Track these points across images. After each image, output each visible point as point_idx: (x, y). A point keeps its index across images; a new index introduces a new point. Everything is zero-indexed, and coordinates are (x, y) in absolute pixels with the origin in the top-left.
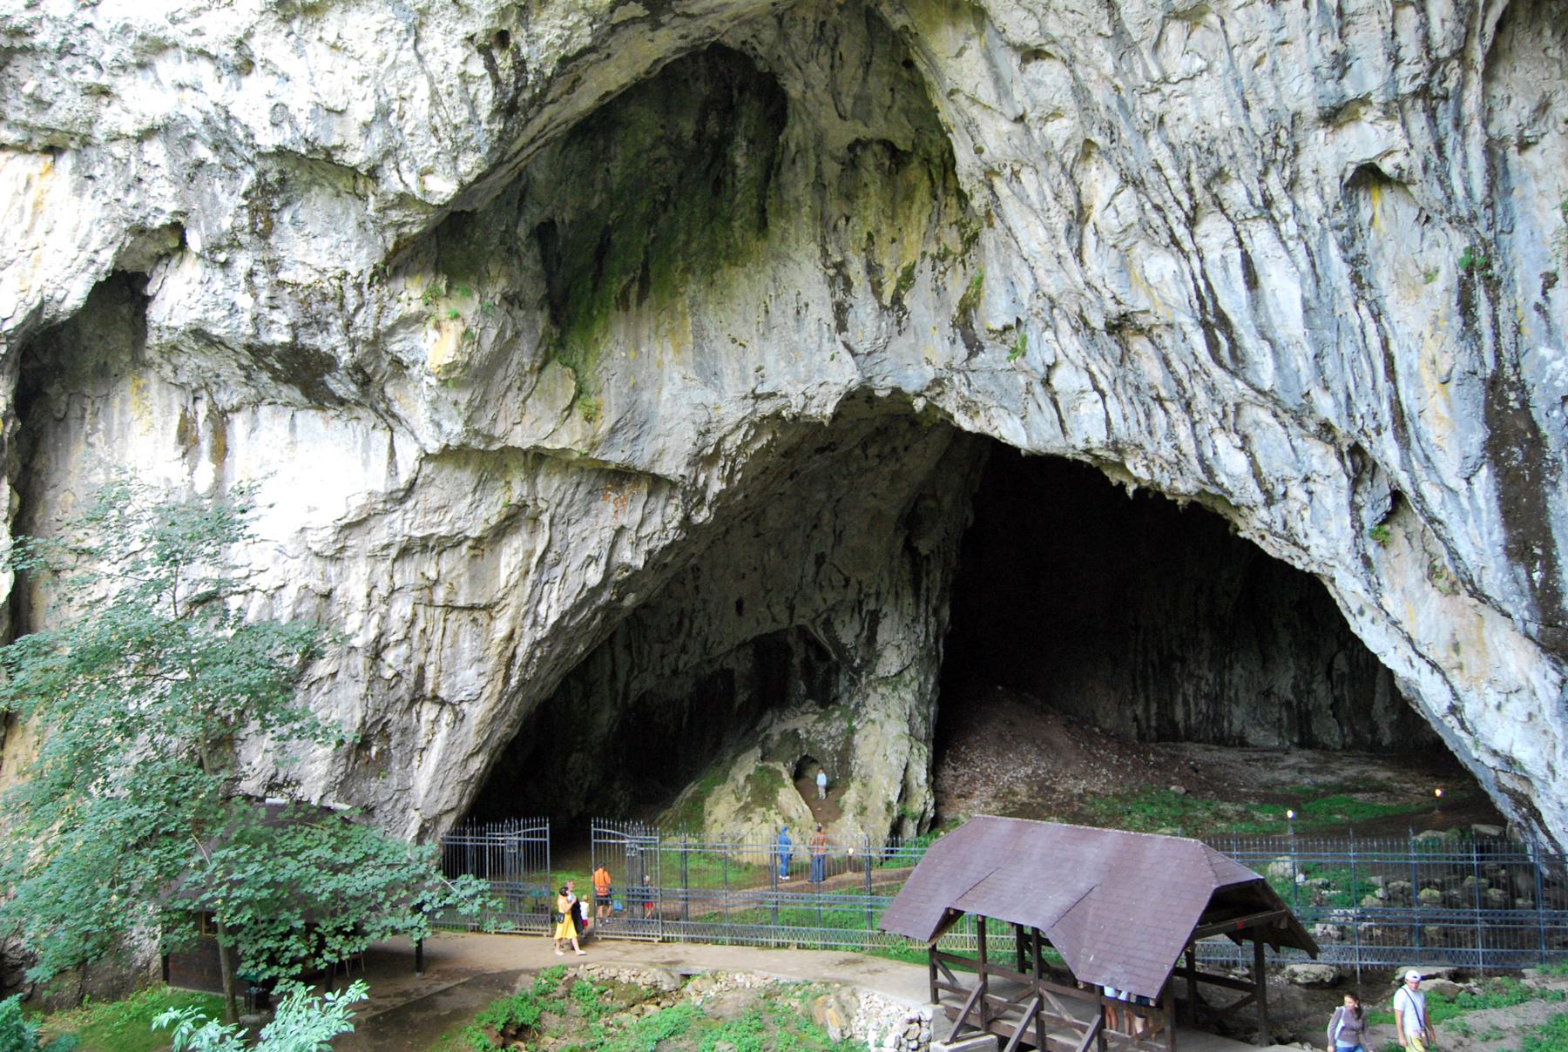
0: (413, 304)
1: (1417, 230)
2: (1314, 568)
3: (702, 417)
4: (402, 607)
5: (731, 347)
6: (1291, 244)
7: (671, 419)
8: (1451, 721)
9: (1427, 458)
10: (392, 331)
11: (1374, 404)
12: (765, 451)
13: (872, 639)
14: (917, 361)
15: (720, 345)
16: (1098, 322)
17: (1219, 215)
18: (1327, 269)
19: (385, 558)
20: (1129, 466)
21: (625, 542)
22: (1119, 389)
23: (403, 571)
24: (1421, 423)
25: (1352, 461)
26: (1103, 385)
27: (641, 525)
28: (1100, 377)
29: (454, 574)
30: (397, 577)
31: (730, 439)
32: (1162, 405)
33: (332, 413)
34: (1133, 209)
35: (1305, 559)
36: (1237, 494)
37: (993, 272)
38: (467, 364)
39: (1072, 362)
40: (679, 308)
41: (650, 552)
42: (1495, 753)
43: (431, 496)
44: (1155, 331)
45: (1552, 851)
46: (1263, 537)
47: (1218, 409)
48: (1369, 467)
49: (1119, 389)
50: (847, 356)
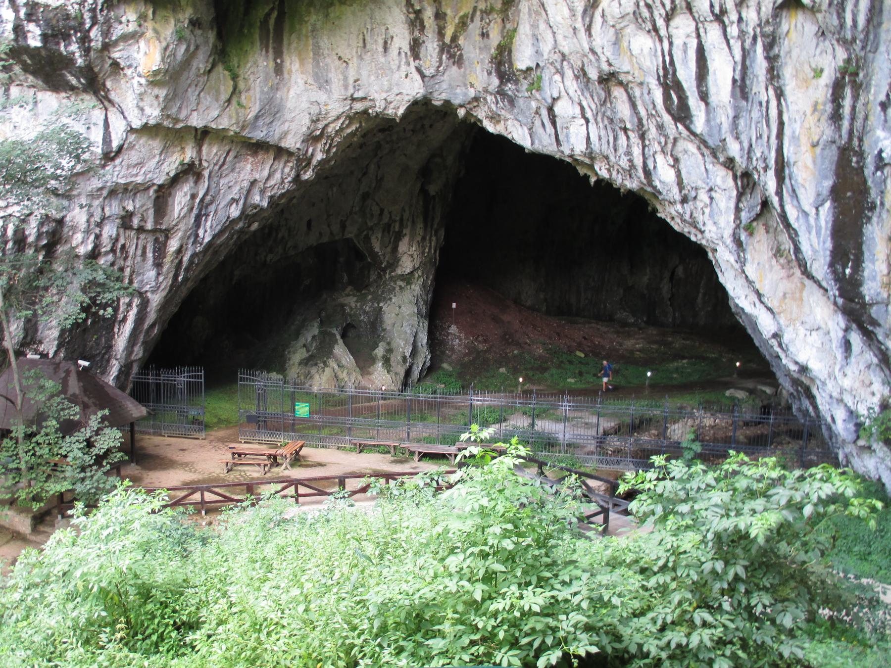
0: (130, 25)
1: (815, 41)
2: (704, 242)
3: (315, 110)
4: (109, 230)
5: (337, 62)
6: (732, 42)
7: (295, 111)
8: (774, 342)
9: (794, 191)
10: (116, 43)
11: (766, 152)
12: (353, 134)
13: (395, 249)
14: (466, 85)
15: (332, 62)
16: (593, 75)
17: (688, 15)
18: (753, 61)
19: (99, 197)
20: (597, 168)
21: (256, 190)
22: (599, 119)
23: (111, 206)
24: (795, 170)
25: (742, 183)
26: (589, 114)
27: (268, 179)
28: (587, 110)
29: (144, 208)
30: (107, 209)
31: (332, 125)
32: (626, 133)
33: (64, 95)
34: (632, 4)
35: (699, 236)
36: (664, 193)
37: (524, 30)
38: (167, 71)
39: (570, 98)
40: (304, 32)
41: (271, 197)
42: (796, 363)
43: (133, 157)
44: (630, 85)
45: (813, 414)
46: (673, 218)
47: (663, 140)
48: (751, 185)
49: (599, 119)
50: (417, 77)
